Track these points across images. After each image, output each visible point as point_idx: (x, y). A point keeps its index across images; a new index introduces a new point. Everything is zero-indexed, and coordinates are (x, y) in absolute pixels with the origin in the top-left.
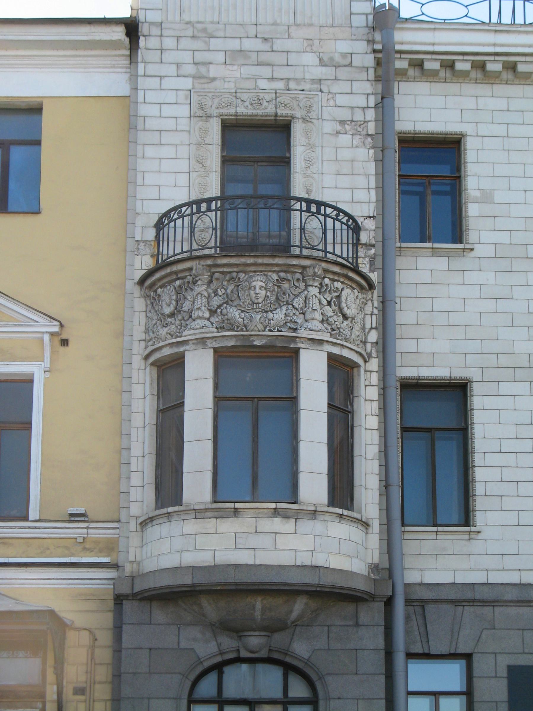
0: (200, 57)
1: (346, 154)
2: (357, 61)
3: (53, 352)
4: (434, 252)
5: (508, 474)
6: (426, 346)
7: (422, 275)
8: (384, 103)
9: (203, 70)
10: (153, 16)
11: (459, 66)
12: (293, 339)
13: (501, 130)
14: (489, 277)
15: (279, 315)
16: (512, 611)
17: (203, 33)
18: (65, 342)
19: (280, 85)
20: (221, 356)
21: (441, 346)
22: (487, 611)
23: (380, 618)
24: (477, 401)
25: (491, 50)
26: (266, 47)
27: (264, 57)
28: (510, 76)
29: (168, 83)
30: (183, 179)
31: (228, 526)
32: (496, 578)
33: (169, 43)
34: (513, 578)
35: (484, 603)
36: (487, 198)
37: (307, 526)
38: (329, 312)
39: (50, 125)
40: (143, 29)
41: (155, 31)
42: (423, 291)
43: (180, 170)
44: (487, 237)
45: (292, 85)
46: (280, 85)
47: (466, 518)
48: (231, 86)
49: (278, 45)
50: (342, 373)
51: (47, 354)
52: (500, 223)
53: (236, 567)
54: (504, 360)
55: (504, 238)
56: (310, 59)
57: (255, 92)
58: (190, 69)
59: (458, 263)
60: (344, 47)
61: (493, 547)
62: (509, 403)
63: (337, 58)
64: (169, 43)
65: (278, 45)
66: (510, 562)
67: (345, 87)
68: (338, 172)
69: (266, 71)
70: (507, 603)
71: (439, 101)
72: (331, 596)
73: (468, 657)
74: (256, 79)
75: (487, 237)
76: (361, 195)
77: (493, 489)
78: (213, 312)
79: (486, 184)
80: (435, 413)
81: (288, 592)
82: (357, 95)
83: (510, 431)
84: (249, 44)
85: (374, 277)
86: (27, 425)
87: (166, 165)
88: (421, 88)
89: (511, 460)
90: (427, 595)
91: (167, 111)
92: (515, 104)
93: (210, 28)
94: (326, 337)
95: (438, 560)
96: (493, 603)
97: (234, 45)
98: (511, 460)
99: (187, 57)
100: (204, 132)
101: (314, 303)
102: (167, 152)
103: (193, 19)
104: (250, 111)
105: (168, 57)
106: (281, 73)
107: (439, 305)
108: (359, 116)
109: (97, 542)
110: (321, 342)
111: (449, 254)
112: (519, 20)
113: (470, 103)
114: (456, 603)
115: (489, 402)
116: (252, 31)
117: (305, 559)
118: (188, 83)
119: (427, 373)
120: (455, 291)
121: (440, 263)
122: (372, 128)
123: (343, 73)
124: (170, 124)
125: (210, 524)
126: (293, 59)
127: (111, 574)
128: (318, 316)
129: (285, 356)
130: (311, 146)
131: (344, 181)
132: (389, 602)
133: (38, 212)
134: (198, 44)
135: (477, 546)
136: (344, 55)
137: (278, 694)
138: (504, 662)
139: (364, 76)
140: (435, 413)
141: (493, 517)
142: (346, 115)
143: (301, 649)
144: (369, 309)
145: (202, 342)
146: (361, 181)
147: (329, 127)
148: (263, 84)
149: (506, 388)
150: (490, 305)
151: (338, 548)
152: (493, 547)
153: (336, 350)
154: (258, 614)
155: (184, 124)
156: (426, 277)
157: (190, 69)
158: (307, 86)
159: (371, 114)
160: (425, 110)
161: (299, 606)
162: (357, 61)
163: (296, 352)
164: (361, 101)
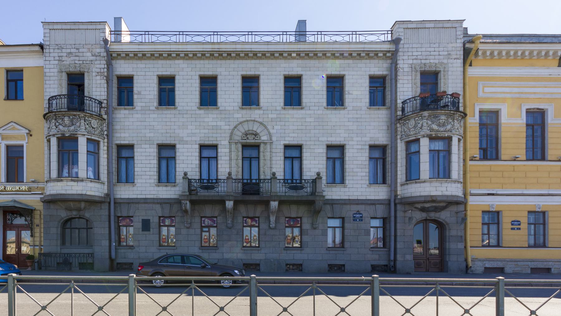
0: (60, 54)
1: (99, 82)
2: (102, 55)
3: (28, 138)
4: (125, 109)
5: (143, 169)
6: (123, 135)
7: (122, 115)
8: (109, 66)
9: (61, 58)
10: (47, 43)
11: (302, 55)
12: (76, 134)
13: (143, 73)
14: (139, 116)
15: (72, 128)
16: (143, 205)
17: (60, 47)
18: (31, 135)
19: (81, 62)
20: (59, 139)
21: (127, 135)
22: (137, 205)
23: (107, 207)
24: (304, 150)
25: (138, 50)
26: (77, 51)
27: (77, 54)
28: (333, 57)
29: (52, 62)
30: (56, 90)
31: (59, 184)
32: (139, 197)
33: (52, 51)
34: (144, 197)
35: (136, 203)
36: (139, 93)
37: (80, 184)
38: (87, 126)
39: (26, 76)
40: (45, 47)
41: (48, 47)
42: (122, 120)
43: (56, 86)
44: (139, 104)
45: (84, 62)
46: (81, 62)
47: (343, 181)
48: (68, 63)
49: (80, 50)
50: (93, 143)
51: (27, 139)
52: (143, 100)
53: (61, 194)
54: (143, 139)
55: (144, 104)
56: (89, 54)
57: (72, 63)
58: (57, 58)
59: (131, 112)
60: (98, 50)
61: (139, 189)
62: (144, 150)
63: (97, 54)
64: (52, 51)
65: (80, 50)
66: (143, 193)
67: (99, 62)
68: (97, 88)
69: (77, 58)
70: (142, 203)
71: (127, 65)
72: (92, 202)
73: (343, 219)
74: (75, 60)
75: (139, 104)
76: (103, 93)
77: (140, 173)
78: (57, 127)
79: (139, 89)
80: (295, 153)
81: (79, 201)
82: (100, 65)
83: (144, 158)
84: (73, 50)
85: (105, 117)
86: (23, 158)
87: (52, 86)
88: (122, 62)
89: (144, 165)
90: (121, 201)
91: (51, 70)
92: (147, 66)
93: (62, 46)
94: (86, 133)
95: (124, 192)
96: (138, 203)
97: (69, 51)
98: (144, 165)
99: (56, 55)
100: (62, 76)
101: (82, 124)
102: (52, 82)
103: (58, 43)
104: (73, 70)
105: (51, 55)
106: (81, 59)
107: (126, 124)
108: (102, 71)
109: (41, 188)
110: (84, 135)
111: (129, 109)
112: (288, 41)
113: (135, 66)
114: (129, 203)
115: (139, 150)
116: (73, 46)
117: (80, 192)
118: (56, 62)
119: (123, 142)
120: (131, 120)
121: (127, 112)
122: (106, 74)
123: (98, 58)
124: (52, 74)
125: (56, 183)
126: (85, 54)
127: (42, 196)
128: (83, 128)
129: (74, 139)
130: (89, 80)
131: (98, 89)
132: (109, 203)
133: (23, 100)
134: (59, 51)
135: (135, 188)
136: (98, 53)
137: (85, 227)
138: (141, 218)
139: (104, 59)
140: (336, 154)
141: (139, 181)
142: (98, 70)
143: (87, 215)
144: (104, 125)
145: (54, 135)
146: (103, 89)
147: (94, 74)
148: (77, 62)
149: (143, 146)
150: (139, 123)
151: (95, 190)
152: (139, 189)
153: (89, 137)
154: (72, 206)
155: (56, 74)
156: (123, 116)
157: (57, 58)
158: (88, 62)
159: (105, 70)
160: (123, 68)
161: (83, 205)
162: (102, 55)
163: (77, 138)
164: (103, 66)
